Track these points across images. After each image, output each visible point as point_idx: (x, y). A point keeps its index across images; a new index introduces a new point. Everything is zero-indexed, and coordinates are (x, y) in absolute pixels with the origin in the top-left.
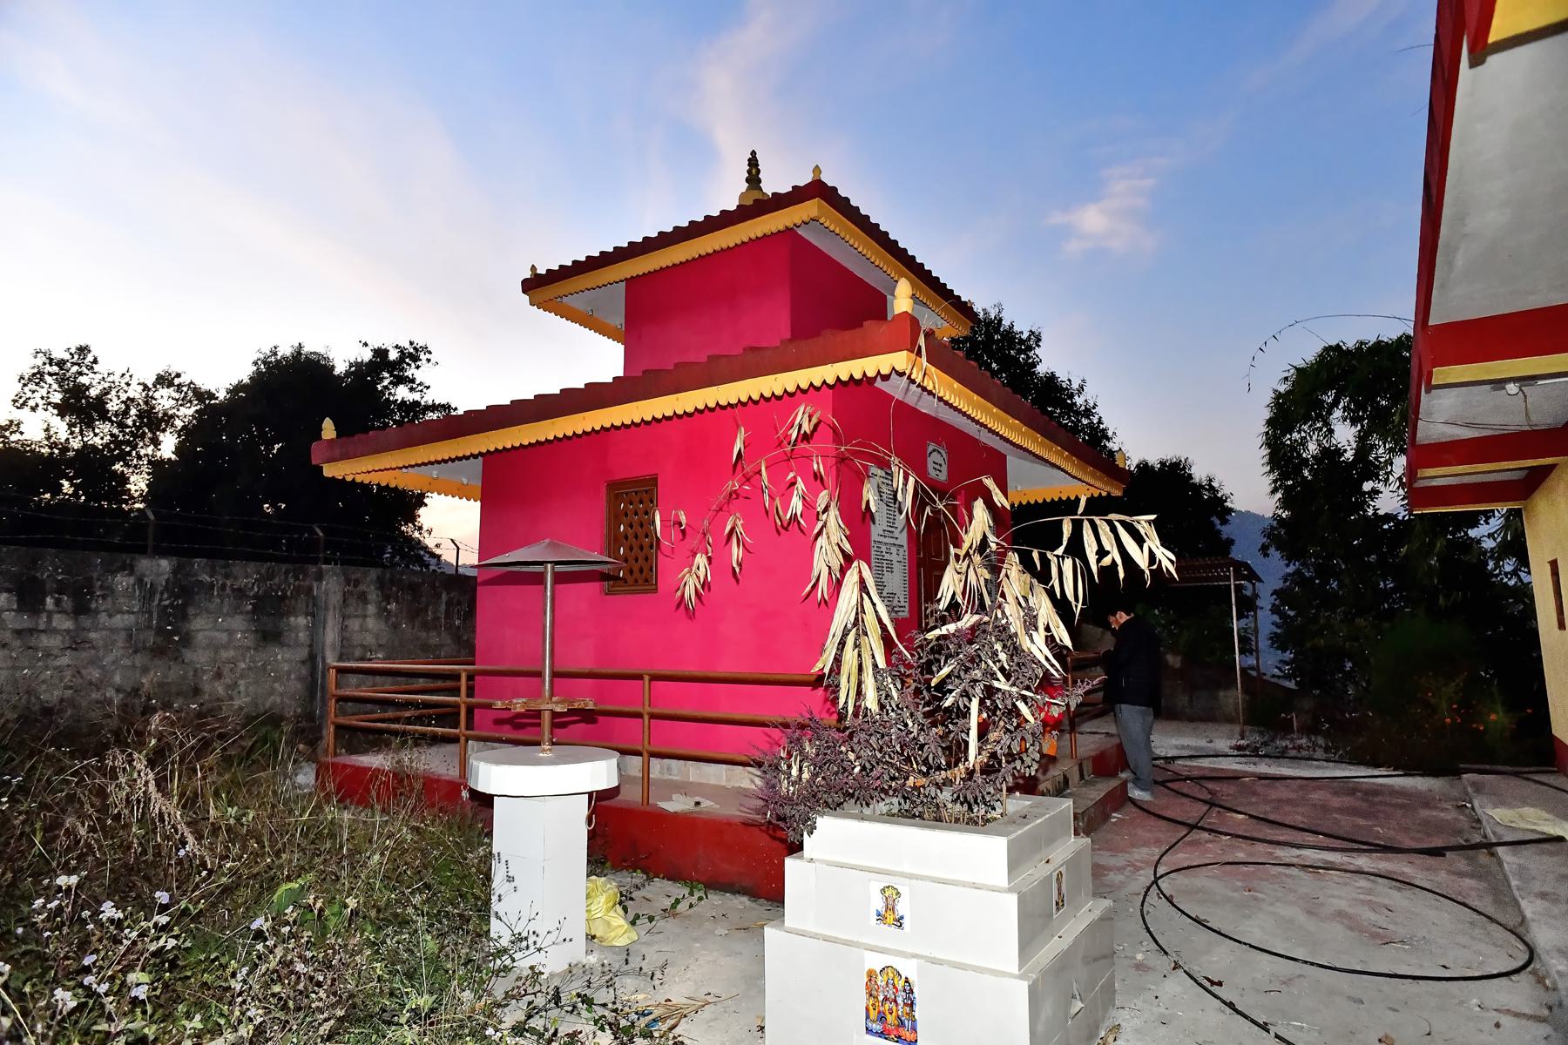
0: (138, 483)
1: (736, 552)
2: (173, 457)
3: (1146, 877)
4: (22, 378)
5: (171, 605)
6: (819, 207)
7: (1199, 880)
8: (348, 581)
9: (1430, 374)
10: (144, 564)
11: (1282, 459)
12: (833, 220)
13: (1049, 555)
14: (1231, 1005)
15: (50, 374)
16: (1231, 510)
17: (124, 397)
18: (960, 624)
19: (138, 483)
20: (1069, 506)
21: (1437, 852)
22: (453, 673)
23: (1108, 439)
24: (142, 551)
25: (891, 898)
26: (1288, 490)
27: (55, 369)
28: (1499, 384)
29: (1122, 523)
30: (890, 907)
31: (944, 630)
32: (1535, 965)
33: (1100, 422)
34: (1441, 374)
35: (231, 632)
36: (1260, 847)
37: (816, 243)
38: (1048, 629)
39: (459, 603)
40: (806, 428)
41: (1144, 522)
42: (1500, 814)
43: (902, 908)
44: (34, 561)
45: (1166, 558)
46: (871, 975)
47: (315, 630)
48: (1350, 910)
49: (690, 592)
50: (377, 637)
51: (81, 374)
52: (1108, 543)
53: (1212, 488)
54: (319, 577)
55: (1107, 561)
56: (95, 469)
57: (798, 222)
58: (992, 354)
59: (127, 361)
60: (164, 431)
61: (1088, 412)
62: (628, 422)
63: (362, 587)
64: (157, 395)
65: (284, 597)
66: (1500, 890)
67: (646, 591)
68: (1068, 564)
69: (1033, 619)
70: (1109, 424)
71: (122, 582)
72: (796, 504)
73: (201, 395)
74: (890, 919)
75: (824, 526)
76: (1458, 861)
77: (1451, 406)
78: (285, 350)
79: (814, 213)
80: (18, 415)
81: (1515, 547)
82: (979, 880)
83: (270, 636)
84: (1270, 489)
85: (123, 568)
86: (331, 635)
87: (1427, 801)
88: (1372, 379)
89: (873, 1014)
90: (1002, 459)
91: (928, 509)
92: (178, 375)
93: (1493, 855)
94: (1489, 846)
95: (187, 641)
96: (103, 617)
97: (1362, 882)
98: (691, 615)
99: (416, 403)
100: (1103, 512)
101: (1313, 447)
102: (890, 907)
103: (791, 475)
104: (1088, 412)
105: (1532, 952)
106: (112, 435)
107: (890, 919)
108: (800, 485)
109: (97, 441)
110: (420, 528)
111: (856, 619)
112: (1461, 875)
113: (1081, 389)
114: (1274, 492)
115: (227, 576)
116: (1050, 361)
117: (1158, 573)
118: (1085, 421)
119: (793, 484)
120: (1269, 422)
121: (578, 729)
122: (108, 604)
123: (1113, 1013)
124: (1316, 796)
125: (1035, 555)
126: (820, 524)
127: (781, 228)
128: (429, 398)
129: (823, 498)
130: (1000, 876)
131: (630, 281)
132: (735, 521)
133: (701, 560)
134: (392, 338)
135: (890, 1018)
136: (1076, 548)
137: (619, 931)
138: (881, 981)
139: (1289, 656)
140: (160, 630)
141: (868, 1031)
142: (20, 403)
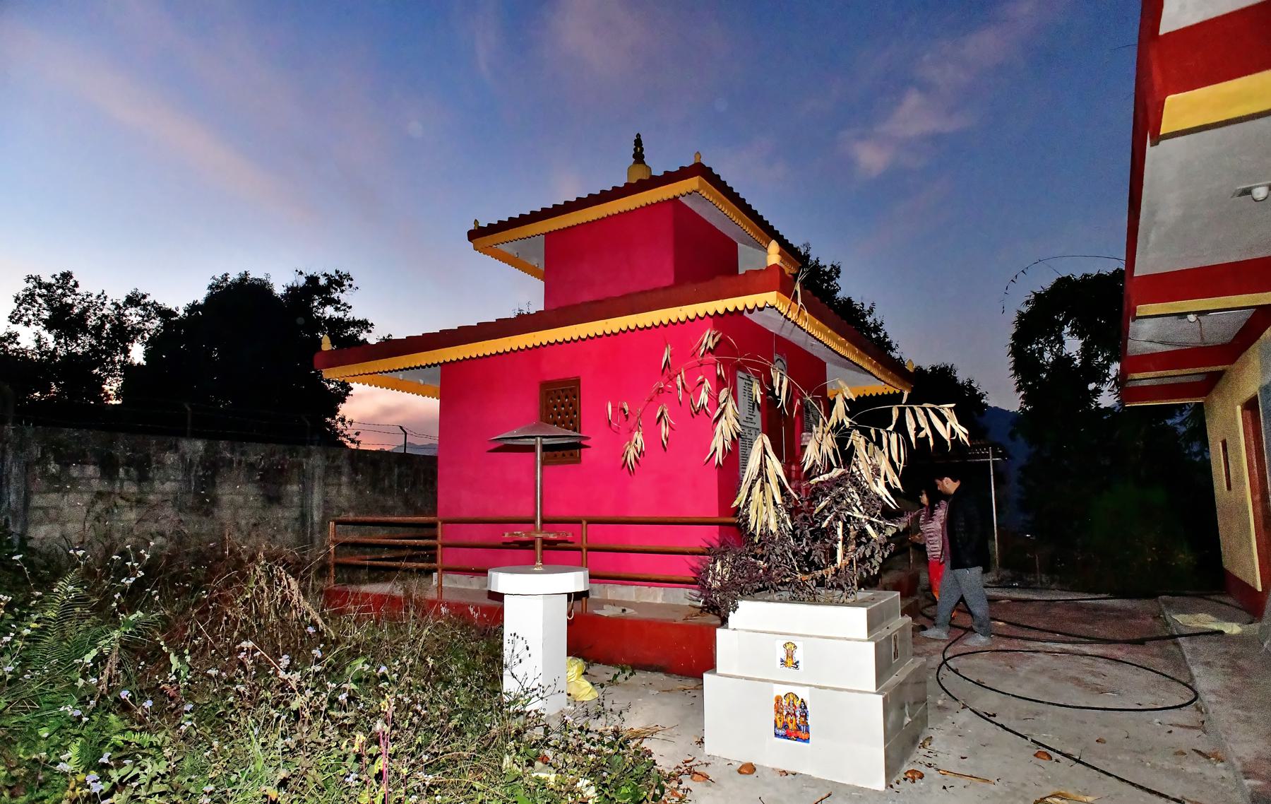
0: (112, 386)
1: (665, 430)
2: (144, 363)
3: (938, 659)
4: (17, 298)
5: (204, 476)
6: (700, 182)
7: (976, 660)
8: (328, 458)
9: (1135, 310)
10: (185, 445)
11: (1025, 365)
12: (709, 192)
13: (882, 431)
14: (1002, 726)
15: (40, 296)
16: (986, 405)
17: (99, 314)
18: (831, 474)
19: (112, 386)
20: (896, 398)
21: (1141, 642)
22: (411, 526)
23: (893, 350)
24: (183, 434)
25: (790, 649)
26: (1028, 388)
27: (44, 291)
28: (1183, 315)
29: (933, 409)
30: (790, 655)
31: (821, 478)
32: (1198, 701)
33: (885, 336)
34: (1142, 309)
35: (246, 496)
36: (1016, 642)
37: (697, 211)
38: (886, 478)
39: (407, 475)
40: (711, 345)
41: (946, 409)
42: (1180, 618)
43: (798, 655)
44: (111, 441)
45: (962, 432)
46: (778, 700)
47: (305, 493)
48: (1080, 676)
49: (631, 457)
50: (349, 500)
51: (64, 295)
52: (923, 422)
53: (973, 390)
54: (308, 455)
55: (922, 434)
56: (78, 374)
57: (684, 192)
58: (814, 285)
59: (103, 282)
60: (132, 342)
61: (877, 329)
62: (568, 339)
63: (338, 462)
64: (127, 312)
65: (283, 469)
66: (1180, 663)
67: (570, 463)
68: (894, 437)
69: (879, 468)
70: (893, 337)
71: (170, 458)
72: (704, 398)
73: (165, 314)
74: (790, 663)
75: (724, 409)
76: (1154, 648)
77: (1149, 329)
78: (234, 276)
79: (696, 187)
80: (15, 328)
81: (1200, 433)
82: (848, 636)
83: (273, 499)
84: (1015, 388)
85: (170, 448)
86: (317, 498)
87: (1133, 615)
88: (1096, 304)
89: (780, 724)
90: (822, 365)
91: (798, 402)
92: (144, 297)
93: (1177, 644)
94: (1173, 637)
95: (215, 502)
96: (157, 484)
97: (1086, 660)
98: (631, 472)
99: (340, 320)
100: (919, 403)
101: (1048, 357)
102: (790, 655)
103: (700, 378)
104: (877, 329)
105: (1196, 693)
106: (91, 345)
107: (790, 663)
108: (707, 384)
109: (80, 350)
110: (343, 420)
111: (761, 470)
112: (1157, 656)
113: (871, 311)
114: (1018, 390)
115: (243, 454)
116: (846, 288)
117: (956, 442)
118: (874, 336)
119: (702, 382)
120: (1015, 337)
121: (555, 554)
122: (161, 474)
123: (926, 730)
124: (1054, 611)
125: (872, 431)
126: (719, 410)
127: (671, 196)
128: (351, 315)
129: (724, 393)
130: (863, 631)
131: (548, 235)
132: (663, 409)
133: (638, 436)
134: (322, 267)
135: (791, 726)
136: (901, 428)
137: (586, 691)
138: (785, 702)
139: (1029, 518)
140: (197, 494)
141: (776, 735)
142: (15, 318)
